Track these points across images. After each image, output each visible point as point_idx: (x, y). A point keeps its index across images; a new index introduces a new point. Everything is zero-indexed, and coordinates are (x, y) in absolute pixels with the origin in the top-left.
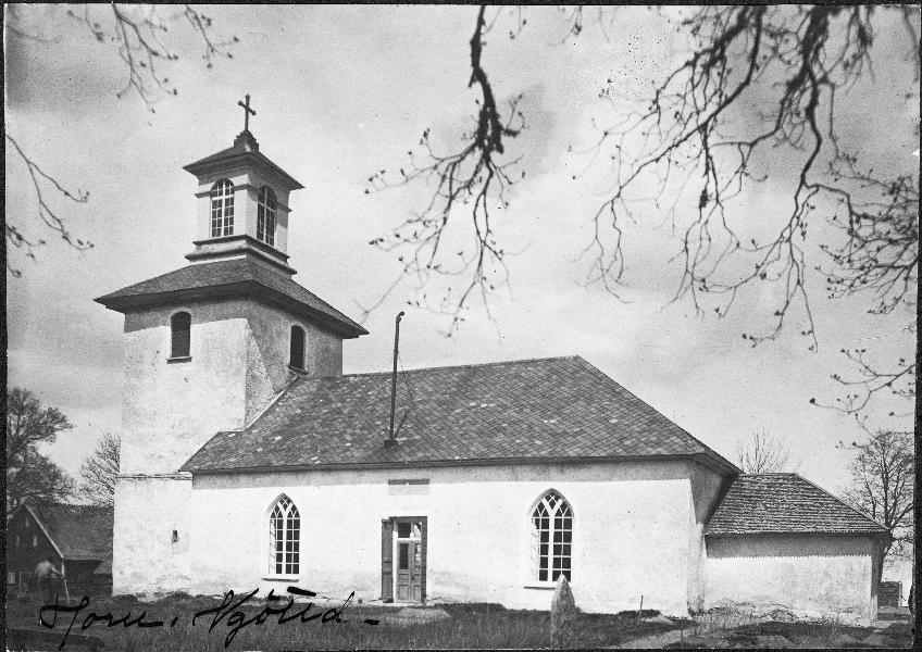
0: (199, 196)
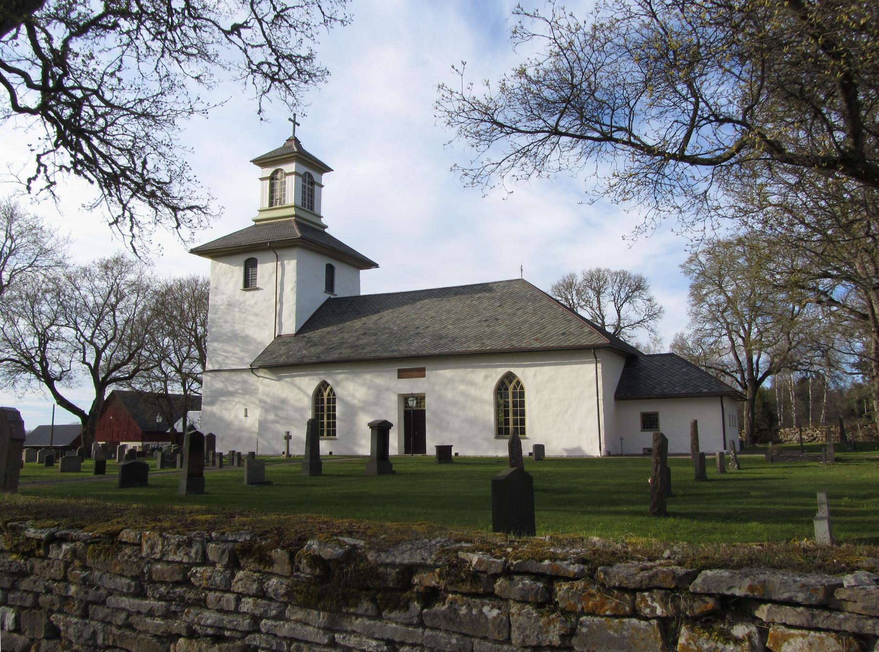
0: (262, 179)
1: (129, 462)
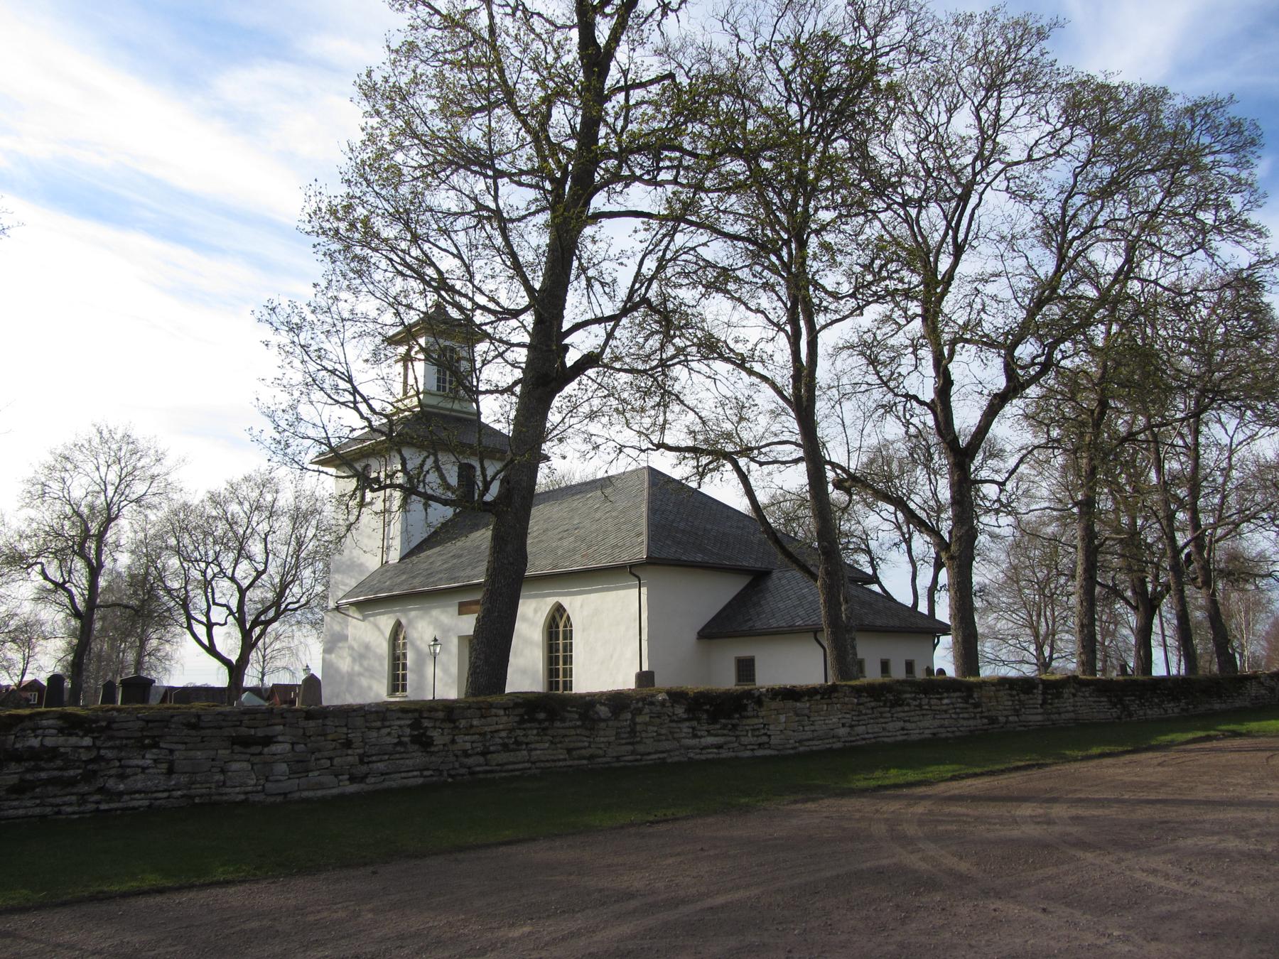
1: (475, 699)
